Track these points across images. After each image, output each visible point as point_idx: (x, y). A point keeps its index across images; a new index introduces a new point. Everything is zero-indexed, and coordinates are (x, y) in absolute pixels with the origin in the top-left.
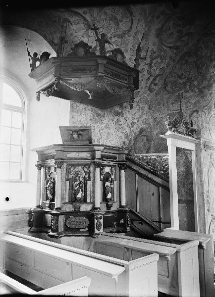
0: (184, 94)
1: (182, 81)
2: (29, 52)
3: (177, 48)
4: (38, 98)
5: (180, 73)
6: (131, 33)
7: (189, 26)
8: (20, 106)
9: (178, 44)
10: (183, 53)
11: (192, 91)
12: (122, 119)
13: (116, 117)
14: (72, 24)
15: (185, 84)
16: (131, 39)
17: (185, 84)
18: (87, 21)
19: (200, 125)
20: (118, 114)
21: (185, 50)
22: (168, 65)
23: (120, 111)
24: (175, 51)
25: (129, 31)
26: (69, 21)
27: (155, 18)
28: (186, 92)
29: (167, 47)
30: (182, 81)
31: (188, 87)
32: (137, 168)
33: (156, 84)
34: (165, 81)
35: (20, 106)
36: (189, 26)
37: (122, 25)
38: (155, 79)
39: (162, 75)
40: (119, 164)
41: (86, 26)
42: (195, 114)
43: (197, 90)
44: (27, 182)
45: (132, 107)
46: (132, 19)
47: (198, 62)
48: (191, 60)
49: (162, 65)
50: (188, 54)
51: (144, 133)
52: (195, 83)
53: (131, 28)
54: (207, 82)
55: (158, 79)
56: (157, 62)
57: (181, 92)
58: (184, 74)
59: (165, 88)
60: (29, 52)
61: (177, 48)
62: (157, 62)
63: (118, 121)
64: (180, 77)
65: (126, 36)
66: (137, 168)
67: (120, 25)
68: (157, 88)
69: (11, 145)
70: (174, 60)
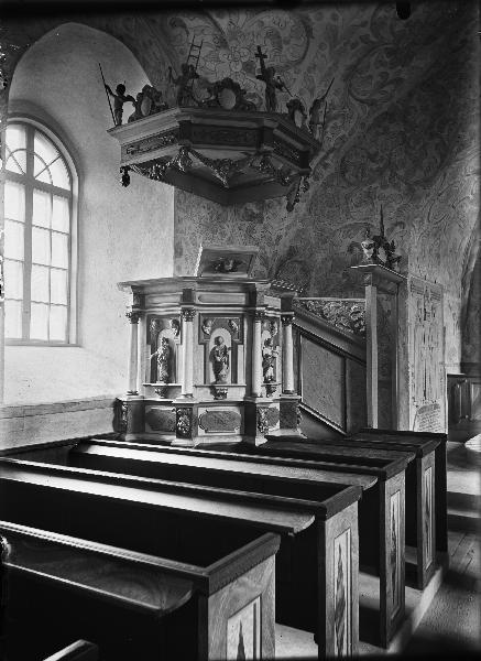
0: (380, 191)
1: (375, 166)
2: (107, 87)
3: (372, 103)
4: (126, 181)
5: (373, 150)
6: (301, 67)
7: (400, 67)
8: (68, 188)
9: (377, 96)
10: (380, 112)
11: (396, 186)
12: (259, 228)
13: (247, 224)
14: (188, 33)
15: (381, 172)
16: (300, 77)
17: (381, 172)
18: (220, 30)
19: (407, 251)
20: (252, 217)
21: (385, 108)
22: (352, 131)
23: (256, 211)
24: (368, 109)
25: (299, 62)
26: (184, 26)
27: (349, 47)
28: (384, 187)
29: (357, 100)
30: (375, 166)
31: (387, 178)
32: (74, 321)
33: (326, 166)
34: (343, 160)
35: (68, 188)
36: (400, 67)
37: (288, 49)
38: (325, 157)
39: (339, 150)
40: (282, 316)
41: (216, 40)
42: (398, 229)
43: (403, 186)
44: (78, 345)
45: (290, 208)
46: (308, 43)
47: (408, 135)
48: (394, 128)
49: (343, 132)
50: (389, 116)
51: (298, 258)
52: (401, 173)
53: (303, 58)
54: (422, 173)
55: (331, 155)
56: (335, 124)
57: (373, 186)
58: (381, 154)
59: (343, 173)
60: (107, 87)
61: (372, 103)
62: (335, 124)
63: (250, 231)
64: (372, 158)
65: (292, 71)
66: (74, 321)
67: (284, 50)
68: (326, 173)
69: (50, 267)
70: (363, 124)
